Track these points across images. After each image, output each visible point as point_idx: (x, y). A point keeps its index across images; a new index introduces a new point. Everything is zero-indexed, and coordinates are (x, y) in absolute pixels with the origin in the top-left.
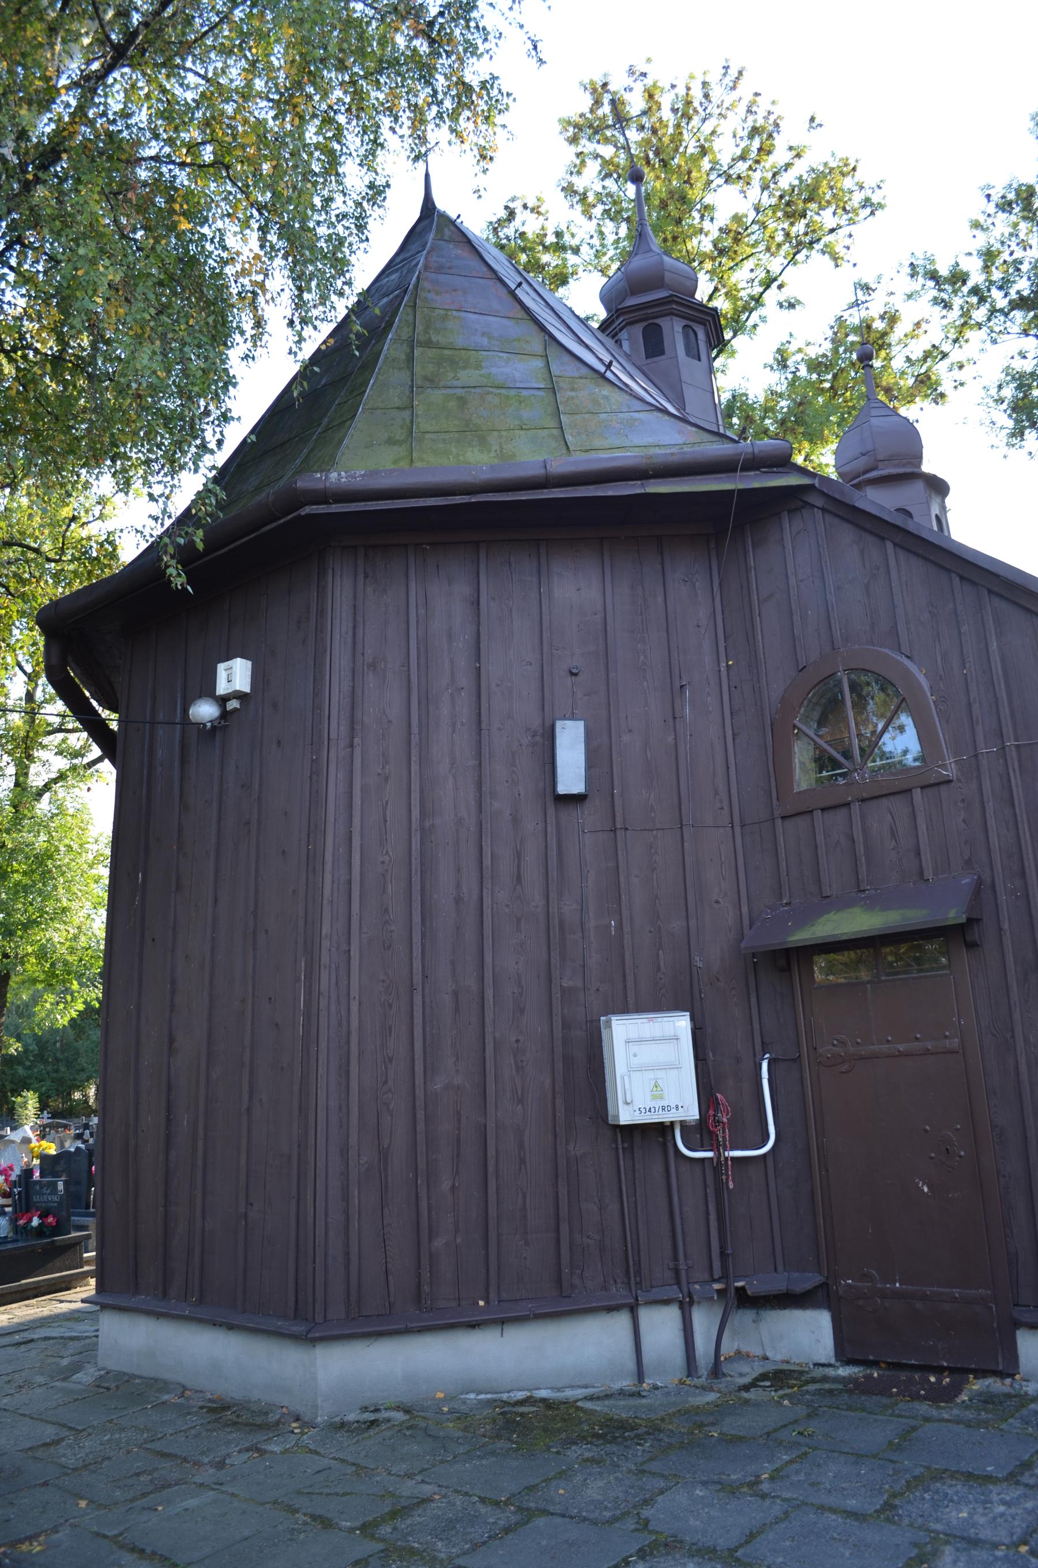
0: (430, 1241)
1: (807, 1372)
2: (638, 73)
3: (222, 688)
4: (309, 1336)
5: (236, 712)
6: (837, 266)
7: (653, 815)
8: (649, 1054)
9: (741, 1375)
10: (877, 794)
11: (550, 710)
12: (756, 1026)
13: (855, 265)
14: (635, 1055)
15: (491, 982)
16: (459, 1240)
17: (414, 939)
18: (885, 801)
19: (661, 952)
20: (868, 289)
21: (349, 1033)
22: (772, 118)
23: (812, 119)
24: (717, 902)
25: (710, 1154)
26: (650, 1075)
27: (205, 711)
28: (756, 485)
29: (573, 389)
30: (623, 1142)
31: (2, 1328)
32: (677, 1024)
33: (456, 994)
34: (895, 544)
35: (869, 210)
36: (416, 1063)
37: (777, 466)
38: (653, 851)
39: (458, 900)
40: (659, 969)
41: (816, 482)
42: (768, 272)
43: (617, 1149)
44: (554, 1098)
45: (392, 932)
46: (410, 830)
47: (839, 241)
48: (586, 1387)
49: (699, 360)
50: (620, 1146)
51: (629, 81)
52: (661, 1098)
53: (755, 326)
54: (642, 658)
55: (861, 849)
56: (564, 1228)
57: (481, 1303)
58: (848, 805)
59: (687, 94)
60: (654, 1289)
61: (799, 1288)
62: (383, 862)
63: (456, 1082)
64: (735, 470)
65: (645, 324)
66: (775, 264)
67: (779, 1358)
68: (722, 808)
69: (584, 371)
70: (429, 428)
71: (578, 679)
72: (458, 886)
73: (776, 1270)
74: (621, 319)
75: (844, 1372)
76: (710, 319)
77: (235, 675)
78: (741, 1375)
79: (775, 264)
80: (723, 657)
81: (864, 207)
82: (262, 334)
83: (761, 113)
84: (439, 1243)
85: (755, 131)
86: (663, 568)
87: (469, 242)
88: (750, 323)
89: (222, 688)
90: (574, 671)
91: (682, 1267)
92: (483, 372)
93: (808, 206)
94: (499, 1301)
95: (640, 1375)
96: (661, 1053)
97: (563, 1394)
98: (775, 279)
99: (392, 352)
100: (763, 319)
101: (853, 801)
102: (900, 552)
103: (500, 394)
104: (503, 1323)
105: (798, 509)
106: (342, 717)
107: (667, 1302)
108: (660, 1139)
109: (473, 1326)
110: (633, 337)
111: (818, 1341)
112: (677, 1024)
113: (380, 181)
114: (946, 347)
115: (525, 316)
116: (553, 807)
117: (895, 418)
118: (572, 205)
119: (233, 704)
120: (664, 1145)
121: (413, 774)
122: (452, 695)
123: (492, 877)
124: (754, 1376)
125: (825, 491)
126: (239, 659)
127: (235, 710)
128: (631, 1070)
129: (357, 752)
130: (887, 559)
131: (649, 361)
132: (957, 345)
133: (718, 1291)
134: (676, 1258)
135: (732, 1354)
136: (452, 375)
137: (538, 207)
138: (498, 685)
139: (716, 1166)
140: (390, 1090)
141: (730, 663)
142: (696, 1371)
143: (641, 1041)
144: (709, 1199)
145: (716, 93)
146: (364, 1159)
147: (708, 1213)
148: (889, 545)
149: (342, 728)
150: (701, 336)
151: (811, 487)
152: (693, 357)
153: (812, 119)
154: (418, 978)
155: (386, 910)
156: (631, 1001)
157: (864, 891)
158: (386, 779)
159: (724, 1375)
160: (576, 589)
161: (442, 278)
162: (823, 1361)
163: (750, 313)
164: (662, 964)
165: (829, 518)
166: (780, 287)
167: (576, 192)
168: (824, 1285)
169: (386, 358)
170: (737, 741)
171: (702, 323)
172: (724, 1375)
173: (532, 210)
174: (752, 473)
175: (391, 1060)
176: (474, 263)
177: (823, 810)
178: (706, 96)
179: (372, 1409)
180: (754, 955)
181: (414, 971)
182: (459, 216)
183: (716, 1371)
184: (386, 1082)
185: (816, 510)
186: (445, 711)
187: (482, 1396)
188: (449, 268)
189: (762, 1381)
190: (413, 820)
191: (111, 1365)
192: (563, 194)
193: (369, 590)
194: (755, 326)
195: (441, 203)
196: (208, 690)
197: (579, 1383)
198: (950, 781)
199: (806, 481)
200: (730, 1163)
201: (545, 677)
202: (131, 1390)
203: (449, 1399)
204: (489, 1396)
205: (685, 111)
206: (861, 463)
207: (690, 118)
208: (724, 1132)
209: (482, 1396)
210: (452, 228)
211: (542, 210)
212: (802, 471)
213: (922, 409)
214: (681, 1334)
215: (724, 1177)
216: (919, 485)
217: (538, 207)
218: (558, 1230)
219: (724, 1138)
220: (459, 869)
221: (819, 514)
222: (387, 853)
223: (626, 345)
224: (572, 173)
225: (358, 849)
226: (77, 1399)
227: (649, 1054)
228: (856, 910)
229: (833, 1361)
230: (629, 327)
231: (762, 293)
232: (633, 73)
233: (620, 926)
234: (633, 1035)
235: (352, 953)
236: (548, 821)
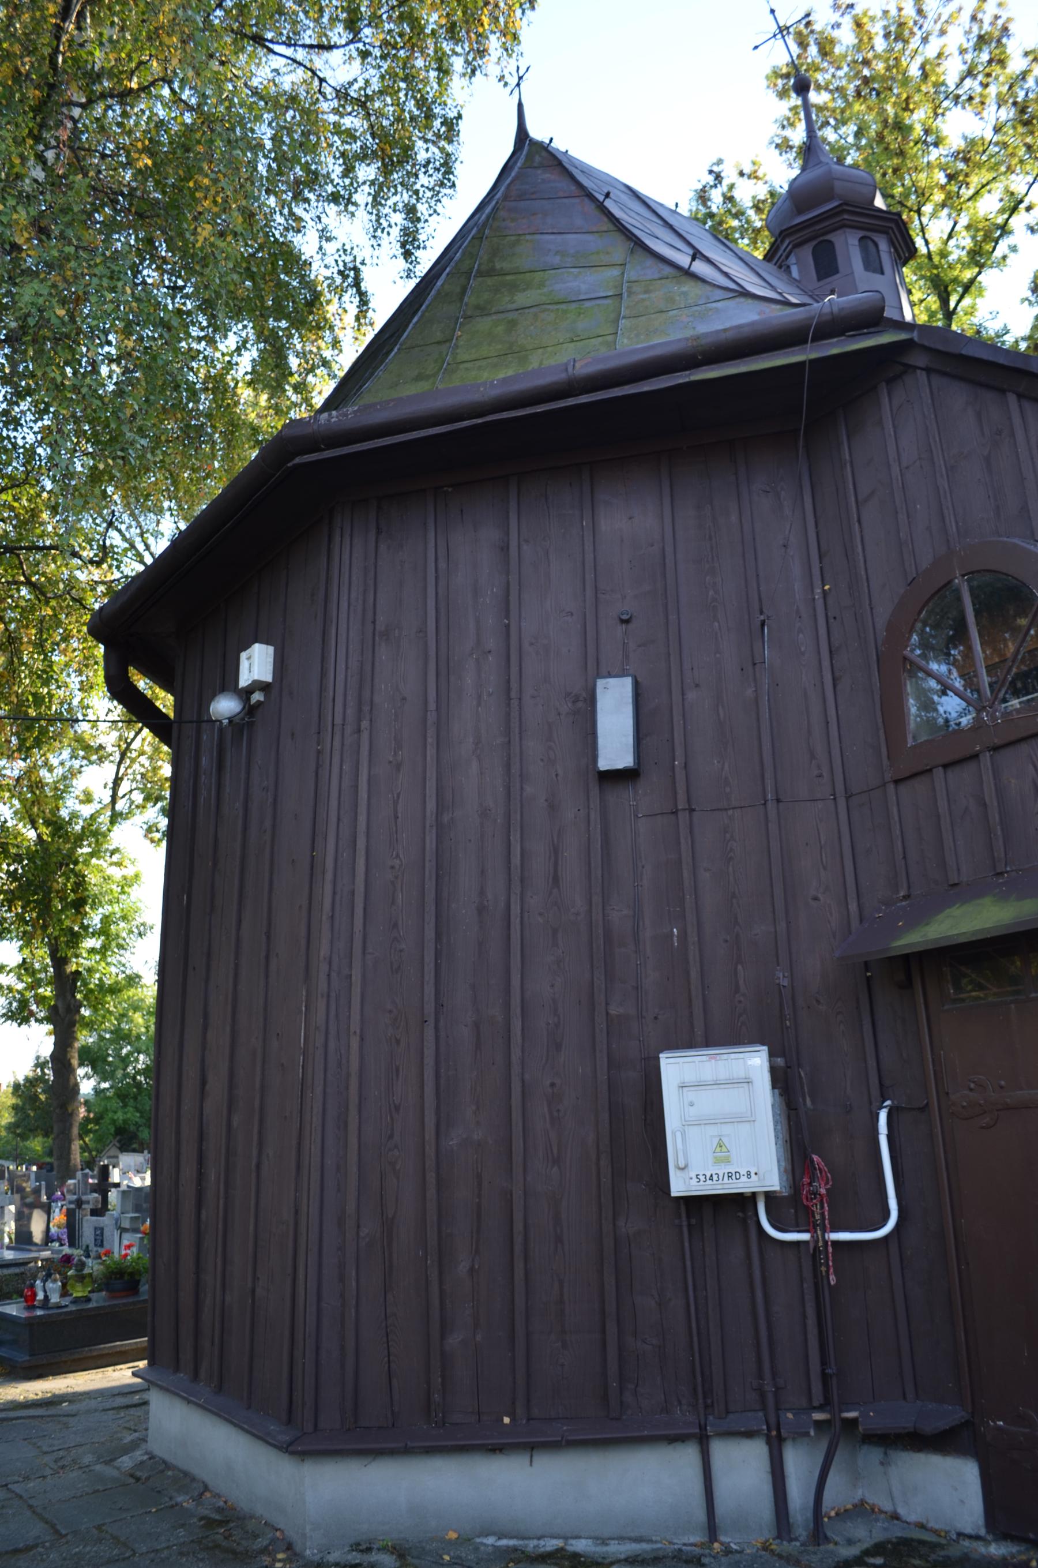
0: (443, 1337)
1: (941, 1546)
2: (844, 6)
3: (245, 680)
4: (291, 1448)
5: (260, 707)
7: (728, 790)
8: (709, 1102)
9: (850, 1542)
10: (1013, 738)
11: (580, 668)
12: (872, 1063)
14: (692, 1104)
15: (519, 1010)
16: (479, 1338)
17: (427, 960)
18: (1024, 748)
19: (740, 967)
21: (348, 1075)
22: (1000, 22)
24: (816, 899)
25: (805, 1237)
26: (712, 1131)
27: (225, 706)
28: (835, 351)
29: (646, 292)
30: (688, 1217)
31: (2, 1407)
32: (749, 1063)
33: (477, 1025)
34: (1020, 396)
36: (426, 1112)
37: (867, 327)
38: (728, 836)
39: (481, 910)
40: (737, 990)
41: (915, 335)
42: (1012, 194)
43: (681, 1226)
44: (598, 1159)
45: (401, 951)
46: (424, 827)
48: (638, 1540)
49: (882, 273)
50: (685, 1223)
51: (835, 17)
52: (727, 1161)
53: (1004, 258)
54: (711, 593)
55: (995, 816)
56: (612, 1329)
57: (507, 1420)
58: (975, 756)
59: (899, 16)
60: (731, 1416)
61: (928, 1428)
62: (392, 867)
63: (475, 1137)
64: (805, 342)
65: (814, 243)
67: (912, 1518)
68: (820, 776)
69: (668, 270)
70: (466, 357)
71: (631, 626)
72: (482, 893)
73: (905, 1398)
74: (787, 242)
75: (996, 1550)
76: (893, 225)
77: (256, 664)
78: (850, 1542)
80: (817, 582)
82: (367, 311)
83: (987, 19)
84: (454, 1340)
85: (982, 40)
86: (737, 479)
87: (560, 163)
88: (998, 253)
89: (245, 680)
90: (625, 617)
91: (769, 1388)
92: (545, 290)
94: (528, 1420)
95: (712, 1529)
96: (730, 1101)
97: (605, 1549)
98: (1021, 201)
99: (446, 287)
100: (1014, 249)
101: (981, 751)
102: (1027, 405)
103: (558, 309)
104: (532, 1449)
105: (898, 377)
106: (349, 698)
107: (749, 1435)
108: (740, 1214)
109: (496, 1449)
111: (962, 1502)
112: (749, 1063)
113: (452, 114)
115: (611, 227)
116: (597, 788)
118: (790, 164)
119: (257, 697)
120: (744, 1221)
121: (428, 758)
122: (477, 660)
123: (522, 880)
124: (866, 1546)
125: (926, 344)
126: (257, 647)
127: (259, 703)
128: (686, 1124)
129: (365, 736)
130: (1010, 418)
131: (822, 283)
133: (818, 1424)
134: (760, 1376)
135: (849, 1506)
136: (507, 299)
137: (755, 172)
138: (532, 644)
139: (813, 1252)
140: (396, 1147)
141: (827, 587)
142: (789, 1532)
143: (699, 1085)
144: (807, 1297)
146: (364, 1231)
147: (804, 1316)
148: (1012, 398)
149: (349, 711)
150: (883, 245)
151: (910, 342)
152: (874, 271)
154: (430, 1008)
155: (396, 925)
156: (699, 1031)
157: (1001, 874)
158: (398, 767)
159: (827, 1540)
160: (630, 520)
161: (522, 204)
162: (968, 1530)
163: (997, 243)
164: (741, 982)
165: (937, 381)
166: (1028, 209)
167: (791, 147)
168: (966, 1424)
169: (439, 292)
170: (839, 687)
171: (883, 231)
172: (827, 1540)
173: (749, 177)
174: (835, 340)
175: (397, 1108)
176: (564, 185)
177: (945, 766)
178: (920, 12)
179: (363, 1547)
180: (867, 966)
181: (426, 999)
182: (551, 139)
183: (818, 1534)
184: (391, 1137)
185: (918, 371)
186: (469, 680)
187: (504, 1542)
188: (533, 193)
189: (873, 1556)
190: (428, 814)
191: (159, 1451)
192: (777, 152)
193: (383, 547)
194: (1004, 258)
195: (537, 132)
196: (228, 682)
197: (632, 1535)
199: (903, 336)
200: (830, 1250)
201: (588, 629)
202: (163, 1481)
203: (464, 1540)
204: (512, 1542)
205: (898, 33)
207: (906, 42)
208: (822, 1207)
209: (504, 1542)
210: (544, 154)
211: (760, 174)
214: (768, 1478)
215: (823, 1269)
217: (755, 172)
218: (603, 1331)
219: (823, 1214)
220: (483, 872)
221: (922, 376)
222: (398, 856)
223: (795, 272)
224: (783, 127)
225: (363, 852)
226: (98, 1491)
227: (709, 1102)
228: (987, 901)
229: (983, 1532)
230: (797, 250)
231: (1008, 220)
232: (839, 7)
233: (683, 935)
234: (690, 1077)
235: (353, 978)
236: (592, 806)
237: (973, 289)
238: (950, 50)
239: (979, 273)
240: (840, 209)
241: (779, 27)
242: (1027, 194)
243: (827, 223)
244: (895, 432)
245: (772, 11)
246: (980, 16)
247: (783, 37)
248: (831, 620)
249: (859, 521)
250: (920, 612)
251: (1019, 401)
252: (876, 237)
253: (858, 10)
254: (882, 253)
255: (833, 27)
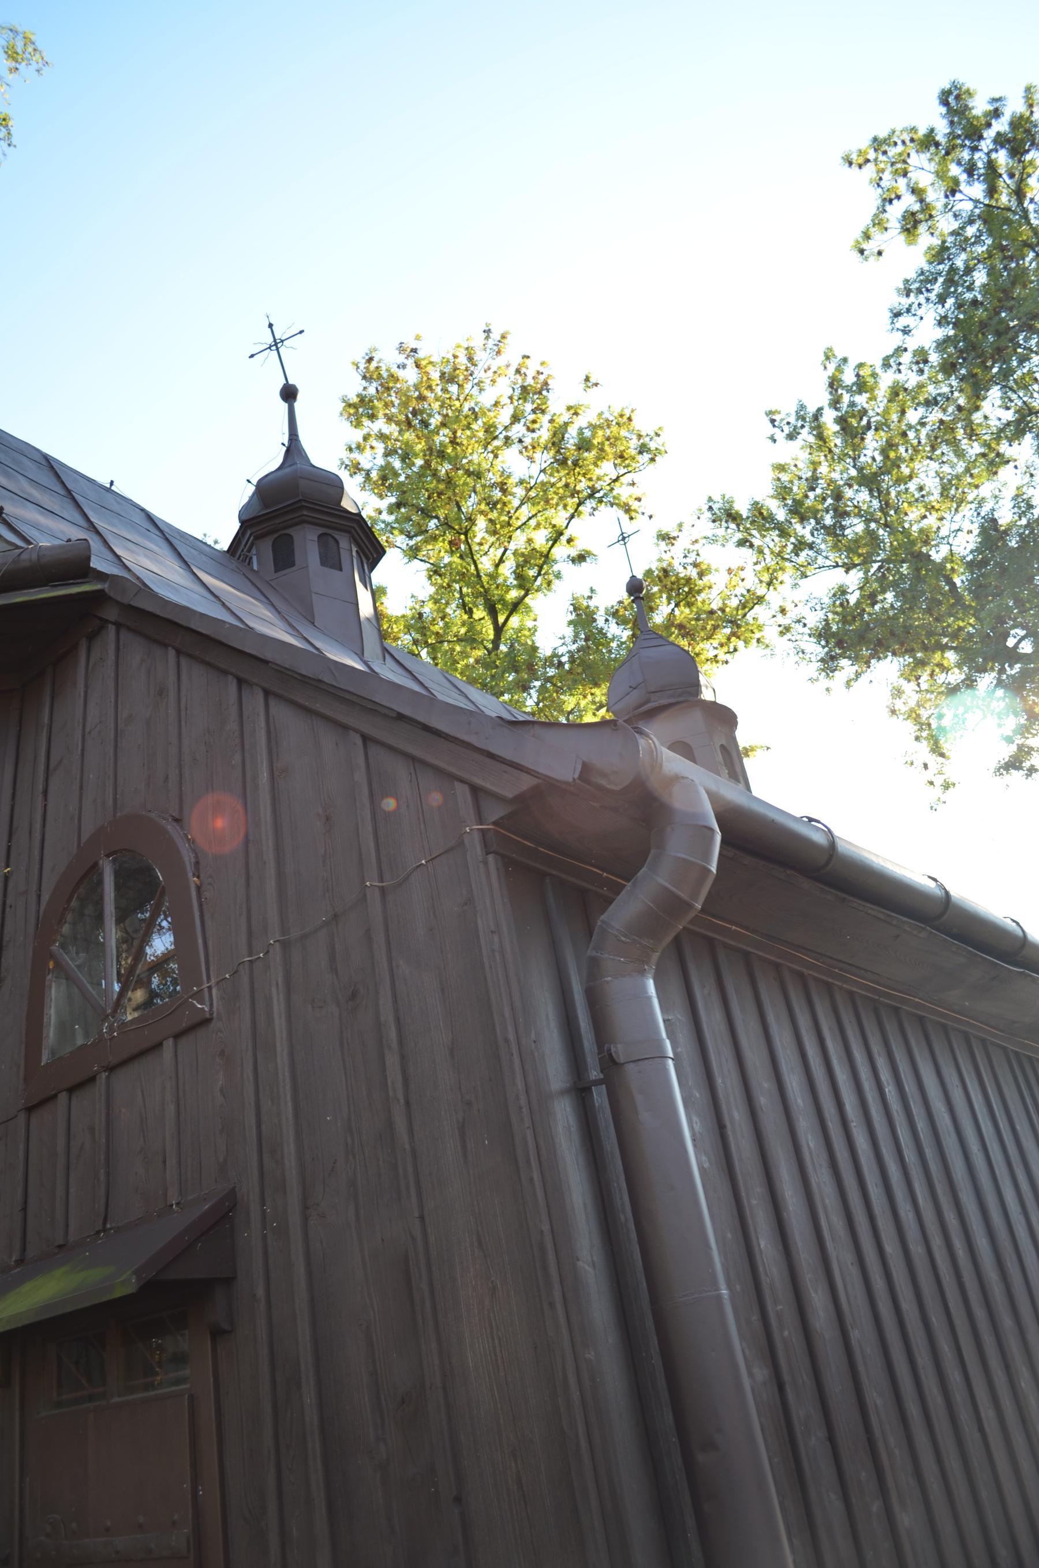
6: (631, 518)
13: (651, 517)
20: (669, 538)
23: (587, 379)
34: (178, 652)
35: (646, 457)
42: (554, 526)
47: (623, 492)
49: (341, 570)
51: (401, 359)
65: (276, 536)
66: (560, 517)
79: (560, 517)
81: (641, 453)
83: (531, 373)
93: (584, 460)
98: (561, 534)
110: (263, 555)
114: (761, 591)
117: (669, 648)
132: (771, 588)
145: (480, 356)
152: (332, 567)
153: (587, 379)
166: (570, 541)
178: (470, 359)
198: (206, 1022)
206: (635, 697)
212: (101, 576)
213: (828, 690)
216: (697, 715)
231: (550, 548)
237: (521, 607)
238: (494, 394)
239: (526, 595)
240: (299, 505)
241: (275, 340)
242: (567, 527)
243: (288, 517)
244: (86, 693)
245: (271, 326)
246: (523, 370)
247: (277, 349)
248: (8, 909)
249: (45, 793)
250: (69, 901)
251: (178, 657)
252: (337, 535)
253: (421, 354)
254: (341, 551)
255: (398, 367)
